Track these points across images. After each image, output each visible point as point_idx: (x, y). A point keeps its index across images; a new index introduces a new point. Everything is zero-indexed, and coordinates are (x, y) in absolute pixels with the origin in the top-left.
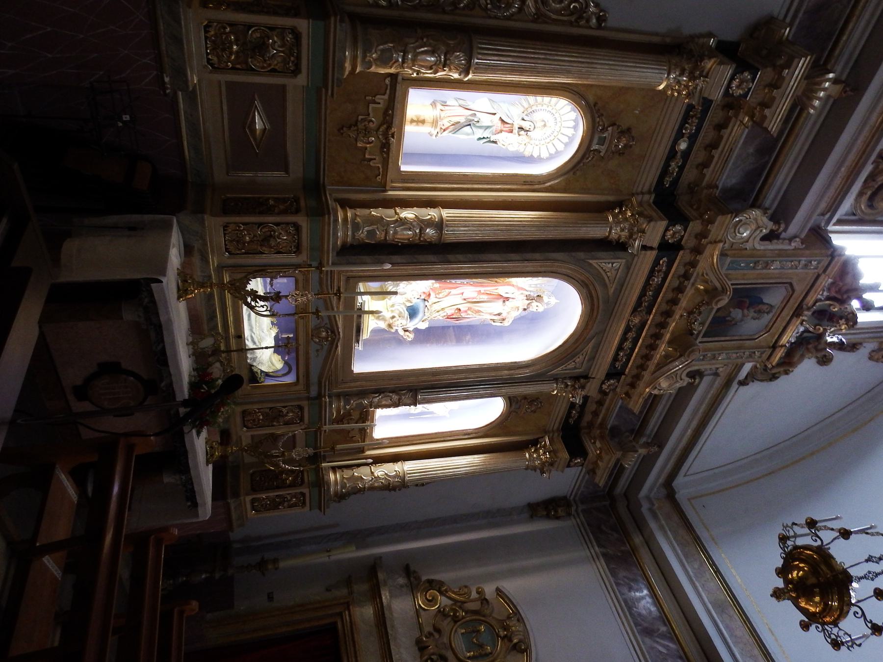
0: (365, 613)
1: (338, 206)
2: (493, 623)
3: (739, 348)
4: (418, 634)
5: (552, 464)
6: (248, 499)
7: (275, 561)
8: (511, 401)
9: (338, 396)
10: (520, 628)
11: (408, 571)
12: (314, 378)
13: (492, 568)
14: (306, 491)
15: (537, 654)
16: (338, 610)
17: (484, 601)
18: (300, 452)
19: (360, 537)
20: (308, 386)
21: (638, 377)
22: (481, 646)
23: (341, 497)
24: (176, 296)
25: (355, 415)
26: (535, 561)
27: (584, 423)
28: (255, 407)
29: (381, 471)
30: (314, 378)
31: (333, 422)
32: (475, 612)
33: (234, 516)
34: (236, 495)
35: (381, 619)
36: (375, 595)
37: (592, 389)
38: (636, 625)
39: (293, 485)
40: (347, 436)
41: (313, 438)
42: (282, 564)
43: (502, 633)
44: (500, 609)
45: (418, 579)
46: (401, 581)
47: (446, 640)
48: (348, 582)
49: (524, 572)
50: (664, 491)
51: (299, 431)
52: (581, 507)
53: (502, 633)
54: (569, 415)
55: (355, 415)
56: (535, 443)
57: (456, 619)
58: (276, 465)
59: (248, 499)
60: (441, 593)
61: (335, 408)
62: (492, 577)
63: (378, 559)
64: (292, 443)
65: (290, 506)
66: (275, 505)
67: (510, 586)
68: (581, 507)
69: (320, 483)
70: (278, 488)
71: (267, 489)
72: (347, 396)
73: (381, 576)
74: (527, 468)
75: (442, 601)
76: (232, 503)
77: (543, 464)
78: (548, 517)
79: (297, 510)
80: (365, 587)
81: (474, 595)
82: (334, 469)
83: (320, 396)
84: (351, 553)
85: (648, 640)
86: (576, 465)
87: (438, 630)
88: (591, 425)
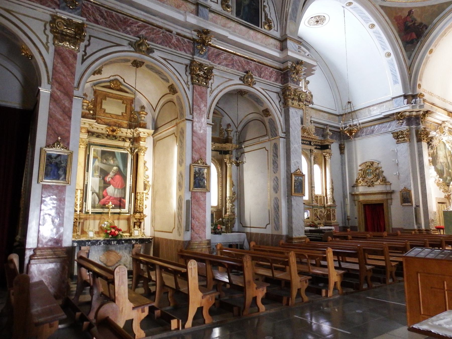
0: (361, 198)
1: (123, 172)
2: (367, 168)
3: (305, 114)
4: (367, 186)
5: (330, 153)
6: (332, 221)
7: (348, 216)
8: (315, 163)
9: (312, 202)
10: (368, 163)
11: (353, 187)
12: (309, 207)
13: (355, 166)
14: (331, 209)
15: (375, 160)
16: (360, 204)
17: (361, 170)
18: (323, 210)
19: (345, 197)
20: (310, 208)
21: (311, 138)
22: (371, 173)
23: (334, 202)
24: (134, 321)
25: (316, 198)
26: (354, 155)
27: (320, 144)
28: (314, 218)
29: (329, 192)
30: (309, 207)
31: (318, 203)
32: (364, 172)
33: (336, 224)
34: (331, 223)
35: (363, 194)
36: (357, 195)
37: (313, 148)
38: (371, 134)
39: (330, 212)
40: (321, 200)
41: (321, 207)
42: (348, 215)
43: (369, 167)
44: (363, 167)
45: (355, 184)
46: (355, 188)
47: (369, 180)
48: (354, 200)
49: (356, 159)
50: (340, 117)
51: (319, 210)
52: (342, 141)
53: (369, 167)
54: (319, 149)
55: (316, 198)
56: (324, 156)
57: (365, 177)
58: (325, 215)
59: (332, 221)
60: (359, 180)
61: (315, 203)
62: (357, 168)
63: (350, 193)
64: (321, 211)
65: (335, 213)
66: (334, 216)
67: (359, 163)
68: (342, 141)
69: (330, 206)
70: (330, 215)
71: (331, 217)
72: (312, 200)
73: (353, 193)
74: (330, 159)
75: (361, 179)
76: (333, 224)
77: (330, 155)
78: (344, 150)
79: (336, 211)
80: (356, 197)
81: (360, 172)
82: (327, 203)
83: (312, 206)
84: (348, 200)
85: (375, 132)
86: (330, 147)
87: (367, 182)
88: (321, 143)
